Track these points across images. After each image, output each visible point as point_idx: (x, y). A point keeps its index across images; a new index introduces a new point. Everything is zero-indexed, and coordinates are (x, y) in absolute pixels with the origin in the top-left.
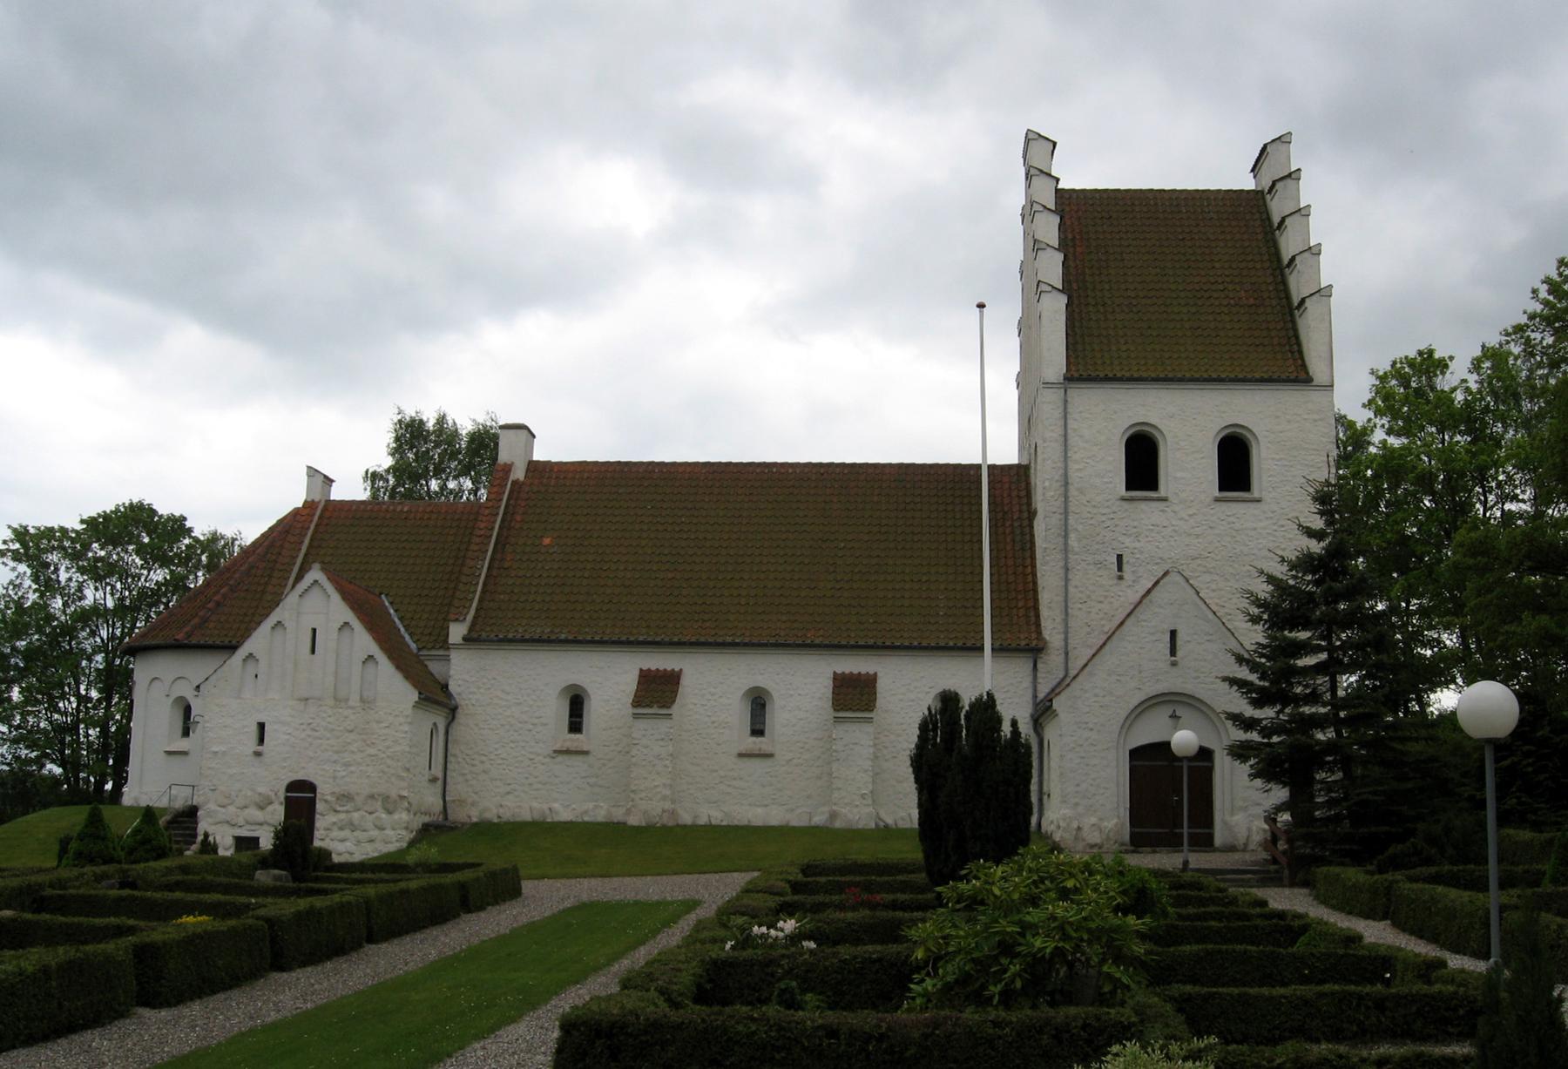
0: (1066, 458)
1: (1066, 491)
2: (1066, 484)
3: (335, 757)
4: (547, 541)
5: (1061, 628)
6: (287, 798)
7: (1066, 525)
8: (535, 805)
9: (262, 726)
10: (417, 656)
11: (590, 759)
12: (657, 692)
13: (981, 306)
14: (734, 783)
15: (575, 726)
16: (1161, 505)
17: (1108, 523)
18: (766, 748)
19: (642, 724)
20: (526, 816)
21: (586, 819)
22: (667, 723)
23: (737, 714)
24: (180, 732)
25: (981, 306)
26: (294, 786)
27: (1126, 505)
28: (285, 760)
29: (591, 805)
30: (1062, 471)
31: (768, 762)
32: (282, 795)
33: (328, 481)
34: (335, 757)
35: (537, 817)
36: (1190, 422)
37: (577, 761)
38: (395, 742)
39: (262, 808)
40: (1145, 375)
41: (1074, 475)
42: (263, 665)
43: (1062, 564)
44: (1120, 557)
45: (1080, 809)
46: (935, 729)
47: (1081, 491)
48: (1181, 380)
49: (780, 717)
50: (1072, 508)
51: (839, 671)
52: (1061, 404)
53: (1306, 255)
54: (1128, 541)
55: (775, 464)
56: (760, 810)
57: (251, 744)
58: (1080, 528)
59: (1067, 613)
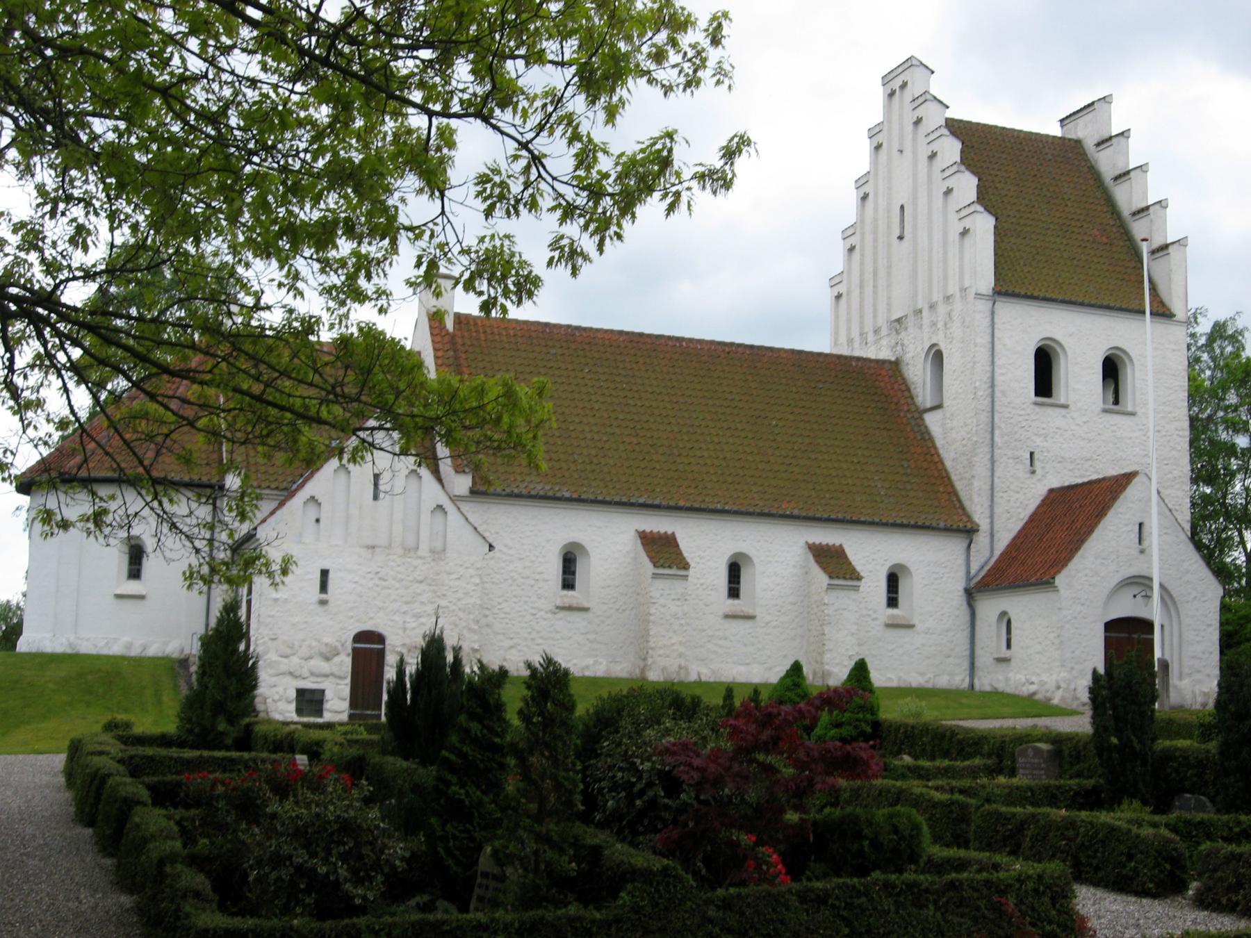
2: (993, 386)
3: (405, 608)
5: (987, 513)
6: (354, 649)
9: (325, 573)
11: (589, 615)
14: (721, 642)
16: (1063, 411)
17: (1024, 424)
18: (748, 610)
19: (660, 584)
21: (587, 674)
24: (331, 575)
26: (361, 637)
27: (1037, 409)
28: (352, 609)
29: (591, 661)
30: (989, 375)
32: (349, 645)
34: (405, 608)
36: (1083, 336)
37: (575, 617)
38: (466, 594)
39: (328, 659)
40: (1112, 304)
43: (988, 456)
44: (1032, 454)
45: (1075, 673)
47: (1003, 392)
48: (1082, 304)
49: (757, 582)
50: (997, 408)
51: (811, 542)
52: (988, 314)
53: (1157, 207)
54: (1038, 440)
56: (742, 669)
57: (315, 594)
58: (1003, 426)
59: (992, 500)
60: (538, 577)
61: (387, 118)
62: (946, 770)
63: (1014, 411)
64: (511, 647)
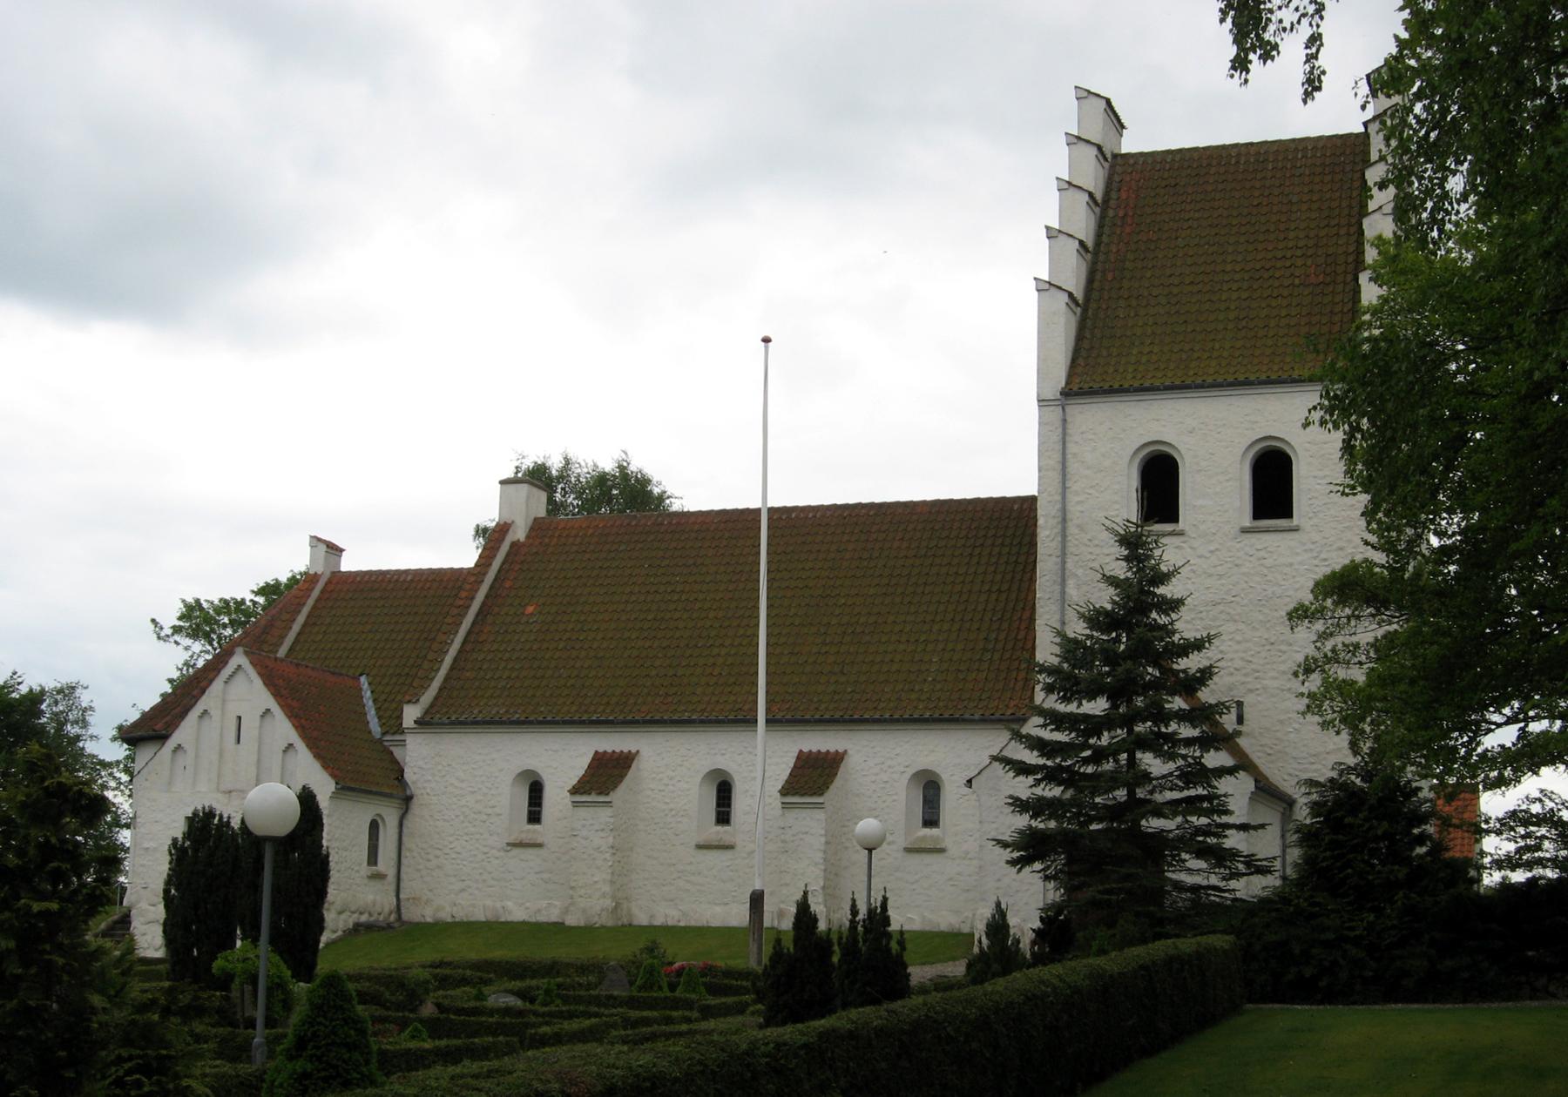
0: (1064, 488)
1: (1064, 529)
2: (1064, 520)
4: (530, 609)
7: (1063, 569)
8: (489, 903)
10: (380, 741)
12: (812, 778)
13: (766, 340)
15: (723, 818)
18: (727, 840)
20: (480, 916)
22: (608, 811)
23: (902, 802)
25: (766, 340)
29: (544, 903)
30: (1059, 506)
31: (728, 854)
33: (334, 550)
35: (490, 917)
41: (1074, 510)
42: (191, 753)
46: (1207, 813)
47: (1080, 527)
50: (1071, 549)
52: (1058, 423)
55: (795, 508)
56: (718, 909)
58: (1080, 572)
60: (490, 811)
61: (1383, 291)
62: (475, 1034)
63: (1098, 551)
64: (463, 890)
